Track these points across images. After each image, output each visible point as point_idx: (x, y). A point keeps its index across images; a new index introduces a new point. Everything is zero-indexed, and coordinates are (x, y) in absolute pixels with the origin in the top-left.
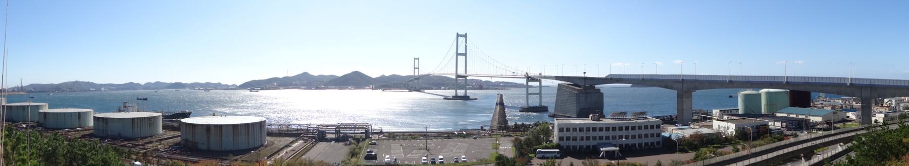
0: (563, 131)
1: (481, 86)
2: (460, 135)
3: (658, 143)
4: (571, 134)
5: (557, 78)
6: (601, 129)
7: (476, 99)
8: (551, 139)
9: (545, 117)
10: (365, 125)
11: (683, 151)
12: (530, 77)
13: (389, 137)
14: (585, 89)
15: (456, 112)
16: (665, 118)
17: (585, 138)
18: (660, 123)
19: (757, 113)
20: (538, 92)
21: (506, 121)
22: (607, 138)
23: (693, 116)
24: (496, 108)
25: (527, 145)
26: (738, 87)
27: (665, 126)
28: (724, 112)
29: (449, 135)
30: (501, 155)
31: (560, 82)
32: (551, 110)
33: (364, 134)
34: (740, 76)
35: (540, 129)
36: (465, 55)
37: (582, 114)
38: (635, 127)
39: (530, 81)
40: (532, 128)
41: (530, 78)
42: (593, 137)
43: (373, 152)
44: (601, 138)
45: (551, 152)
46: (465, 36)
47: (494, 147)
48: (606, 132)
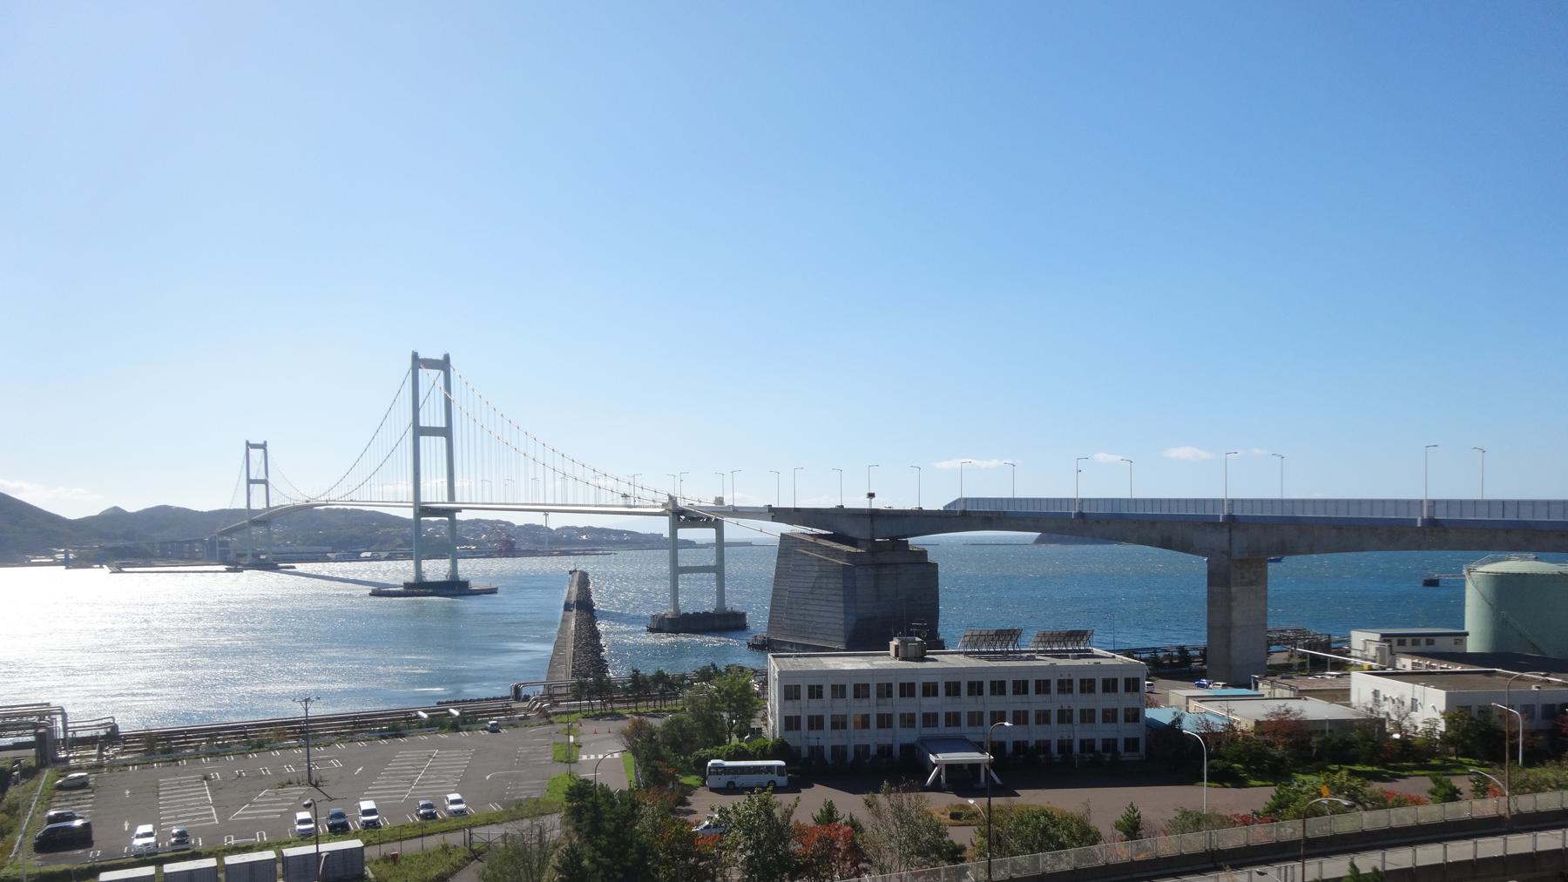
1: (508, 542)
2: (439, 722)
3: (1132, 744)
4: (826, 707)
5: (777, 514)
6: (930, 690)
7: (493, 591)
8: (756, 723)
9: (733, 651)
10: (32, 714)
11: (1225, 777)
12: (683, 512)
13: (150, 752)
14: (871, 552)
15: (420, 639)
16: (1161, 655)
17: (873, 721)
18: (1141, 675)
19: (1552, 656)
20: (712, 562)
21: (600, 666)
22: (953, 719)
23: (1269, 654)
24: (565, 621)
25: (676, 746)
26: (1465, 546)
27: (1161, 685)
28: (1402, 643)
29: (397, 726)
30: (586, 781)
32: (759, 622)
33: (33, 751)
34: (1475, 502)
35: (719, 691)
36: (446, 432)
37: (864, 638)
38: (1047, 682)
39: (685, 525)
40: (690, 686)
41: (681, 516)
42: (902, 716)
43: (73, 818)
44: (930, 719)
45: (757, 770)
46: (444, 365)
47: (561, 756)
48: (949, 699)
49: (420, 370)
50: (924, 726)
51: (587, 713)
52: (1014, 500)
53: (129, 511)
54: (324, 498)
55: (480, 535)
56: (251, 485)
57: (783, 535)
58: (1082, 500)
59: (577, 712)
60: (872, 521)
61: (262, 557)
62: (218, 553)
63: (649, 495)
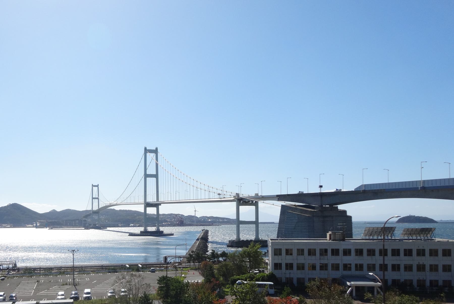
0: (280, 254)
4: (293, 259)
5: (280, 198)
7: (172, 235)
13: (25, 273)
22: (359, 267)
24: (195, 243)
31: (283, 203)
44: (347, 267)
46: (155, 151)
49: (147, 154)
50: (344, 270)
51: (192, 268)
52: (389, 184)
53: (58, 211)
54: (115, 203)
55: (171, 219)
56: (93, 200)
57: (282, 205)
58: (424, 181)
59: (189, 267)
60: (321, 197)
61: (97, 225)
62: (83, 223)
63: (229, 194)
